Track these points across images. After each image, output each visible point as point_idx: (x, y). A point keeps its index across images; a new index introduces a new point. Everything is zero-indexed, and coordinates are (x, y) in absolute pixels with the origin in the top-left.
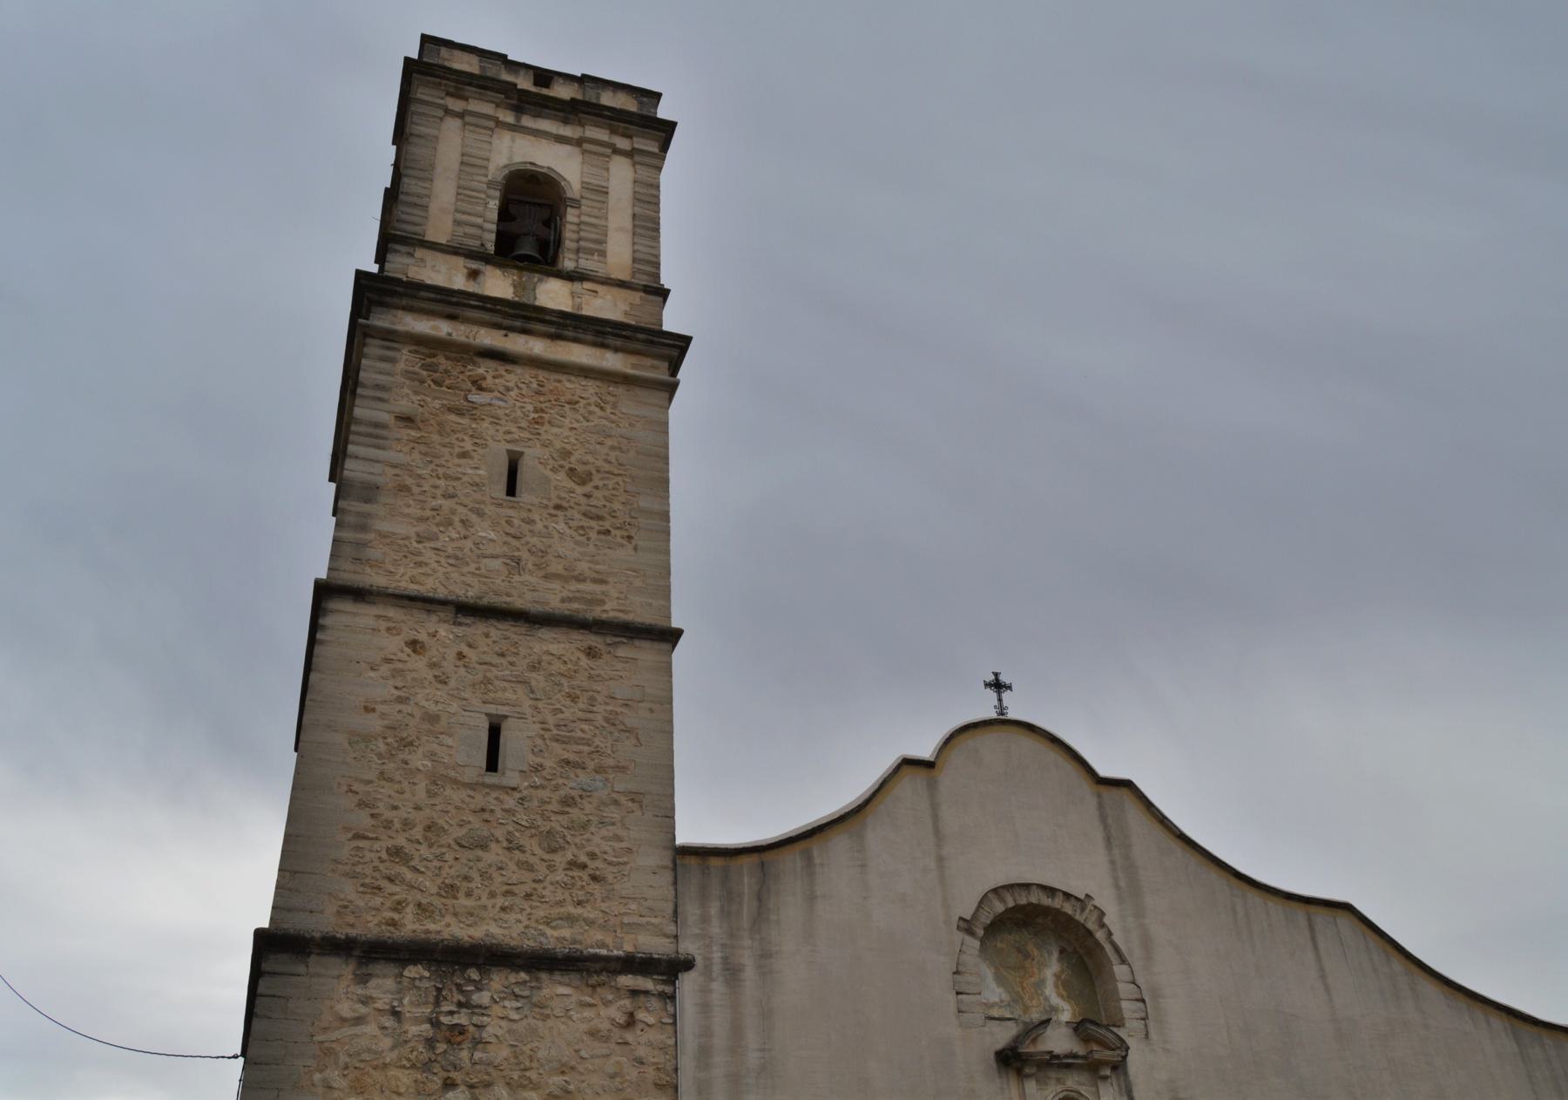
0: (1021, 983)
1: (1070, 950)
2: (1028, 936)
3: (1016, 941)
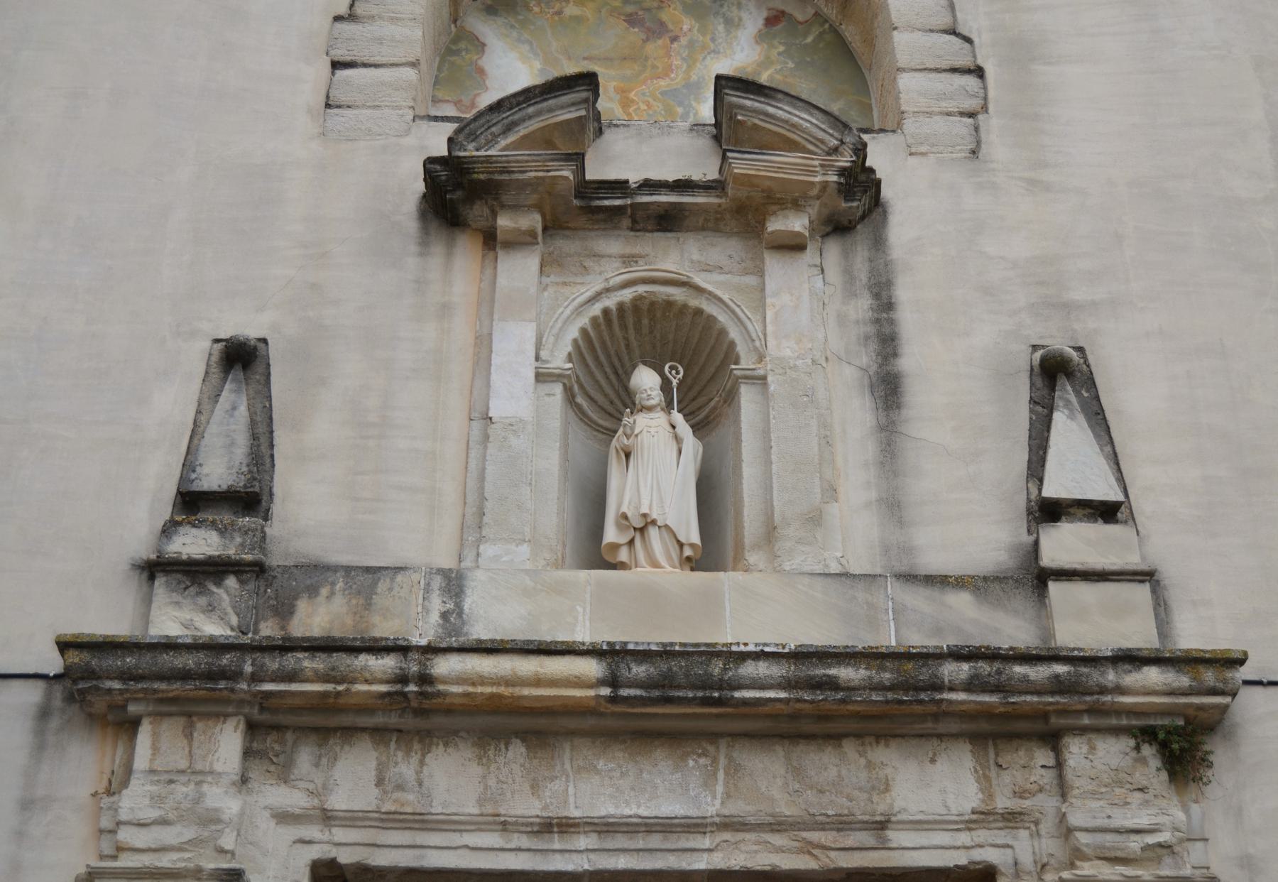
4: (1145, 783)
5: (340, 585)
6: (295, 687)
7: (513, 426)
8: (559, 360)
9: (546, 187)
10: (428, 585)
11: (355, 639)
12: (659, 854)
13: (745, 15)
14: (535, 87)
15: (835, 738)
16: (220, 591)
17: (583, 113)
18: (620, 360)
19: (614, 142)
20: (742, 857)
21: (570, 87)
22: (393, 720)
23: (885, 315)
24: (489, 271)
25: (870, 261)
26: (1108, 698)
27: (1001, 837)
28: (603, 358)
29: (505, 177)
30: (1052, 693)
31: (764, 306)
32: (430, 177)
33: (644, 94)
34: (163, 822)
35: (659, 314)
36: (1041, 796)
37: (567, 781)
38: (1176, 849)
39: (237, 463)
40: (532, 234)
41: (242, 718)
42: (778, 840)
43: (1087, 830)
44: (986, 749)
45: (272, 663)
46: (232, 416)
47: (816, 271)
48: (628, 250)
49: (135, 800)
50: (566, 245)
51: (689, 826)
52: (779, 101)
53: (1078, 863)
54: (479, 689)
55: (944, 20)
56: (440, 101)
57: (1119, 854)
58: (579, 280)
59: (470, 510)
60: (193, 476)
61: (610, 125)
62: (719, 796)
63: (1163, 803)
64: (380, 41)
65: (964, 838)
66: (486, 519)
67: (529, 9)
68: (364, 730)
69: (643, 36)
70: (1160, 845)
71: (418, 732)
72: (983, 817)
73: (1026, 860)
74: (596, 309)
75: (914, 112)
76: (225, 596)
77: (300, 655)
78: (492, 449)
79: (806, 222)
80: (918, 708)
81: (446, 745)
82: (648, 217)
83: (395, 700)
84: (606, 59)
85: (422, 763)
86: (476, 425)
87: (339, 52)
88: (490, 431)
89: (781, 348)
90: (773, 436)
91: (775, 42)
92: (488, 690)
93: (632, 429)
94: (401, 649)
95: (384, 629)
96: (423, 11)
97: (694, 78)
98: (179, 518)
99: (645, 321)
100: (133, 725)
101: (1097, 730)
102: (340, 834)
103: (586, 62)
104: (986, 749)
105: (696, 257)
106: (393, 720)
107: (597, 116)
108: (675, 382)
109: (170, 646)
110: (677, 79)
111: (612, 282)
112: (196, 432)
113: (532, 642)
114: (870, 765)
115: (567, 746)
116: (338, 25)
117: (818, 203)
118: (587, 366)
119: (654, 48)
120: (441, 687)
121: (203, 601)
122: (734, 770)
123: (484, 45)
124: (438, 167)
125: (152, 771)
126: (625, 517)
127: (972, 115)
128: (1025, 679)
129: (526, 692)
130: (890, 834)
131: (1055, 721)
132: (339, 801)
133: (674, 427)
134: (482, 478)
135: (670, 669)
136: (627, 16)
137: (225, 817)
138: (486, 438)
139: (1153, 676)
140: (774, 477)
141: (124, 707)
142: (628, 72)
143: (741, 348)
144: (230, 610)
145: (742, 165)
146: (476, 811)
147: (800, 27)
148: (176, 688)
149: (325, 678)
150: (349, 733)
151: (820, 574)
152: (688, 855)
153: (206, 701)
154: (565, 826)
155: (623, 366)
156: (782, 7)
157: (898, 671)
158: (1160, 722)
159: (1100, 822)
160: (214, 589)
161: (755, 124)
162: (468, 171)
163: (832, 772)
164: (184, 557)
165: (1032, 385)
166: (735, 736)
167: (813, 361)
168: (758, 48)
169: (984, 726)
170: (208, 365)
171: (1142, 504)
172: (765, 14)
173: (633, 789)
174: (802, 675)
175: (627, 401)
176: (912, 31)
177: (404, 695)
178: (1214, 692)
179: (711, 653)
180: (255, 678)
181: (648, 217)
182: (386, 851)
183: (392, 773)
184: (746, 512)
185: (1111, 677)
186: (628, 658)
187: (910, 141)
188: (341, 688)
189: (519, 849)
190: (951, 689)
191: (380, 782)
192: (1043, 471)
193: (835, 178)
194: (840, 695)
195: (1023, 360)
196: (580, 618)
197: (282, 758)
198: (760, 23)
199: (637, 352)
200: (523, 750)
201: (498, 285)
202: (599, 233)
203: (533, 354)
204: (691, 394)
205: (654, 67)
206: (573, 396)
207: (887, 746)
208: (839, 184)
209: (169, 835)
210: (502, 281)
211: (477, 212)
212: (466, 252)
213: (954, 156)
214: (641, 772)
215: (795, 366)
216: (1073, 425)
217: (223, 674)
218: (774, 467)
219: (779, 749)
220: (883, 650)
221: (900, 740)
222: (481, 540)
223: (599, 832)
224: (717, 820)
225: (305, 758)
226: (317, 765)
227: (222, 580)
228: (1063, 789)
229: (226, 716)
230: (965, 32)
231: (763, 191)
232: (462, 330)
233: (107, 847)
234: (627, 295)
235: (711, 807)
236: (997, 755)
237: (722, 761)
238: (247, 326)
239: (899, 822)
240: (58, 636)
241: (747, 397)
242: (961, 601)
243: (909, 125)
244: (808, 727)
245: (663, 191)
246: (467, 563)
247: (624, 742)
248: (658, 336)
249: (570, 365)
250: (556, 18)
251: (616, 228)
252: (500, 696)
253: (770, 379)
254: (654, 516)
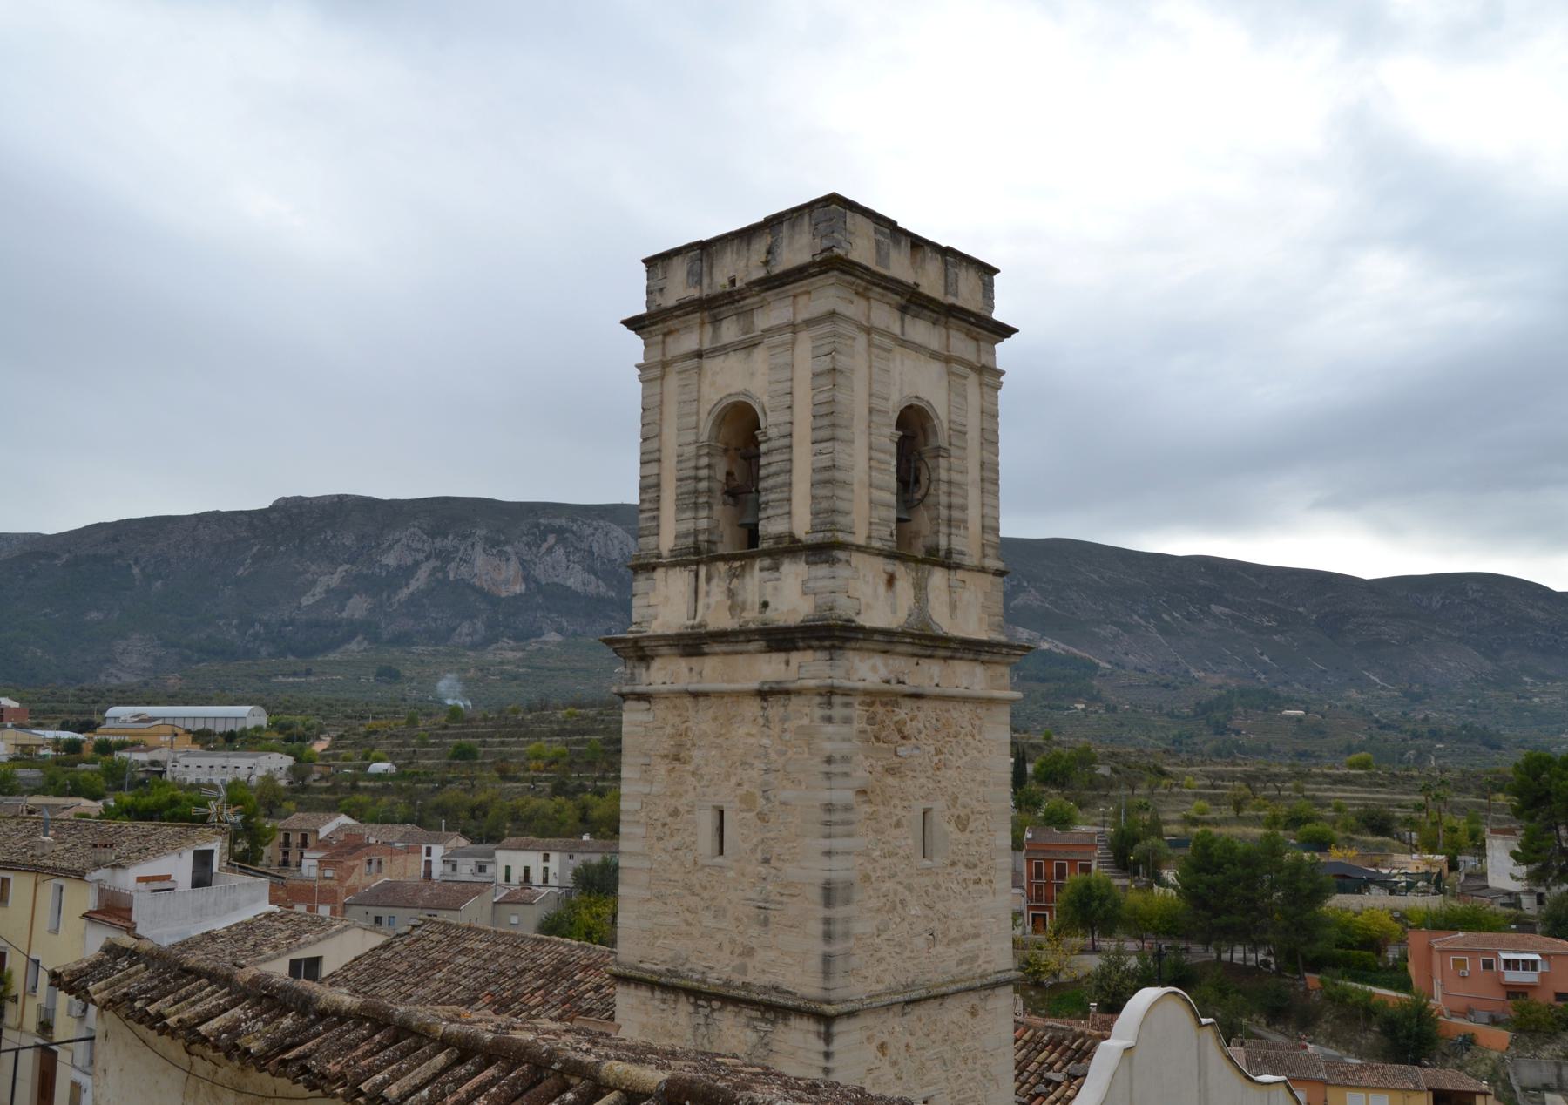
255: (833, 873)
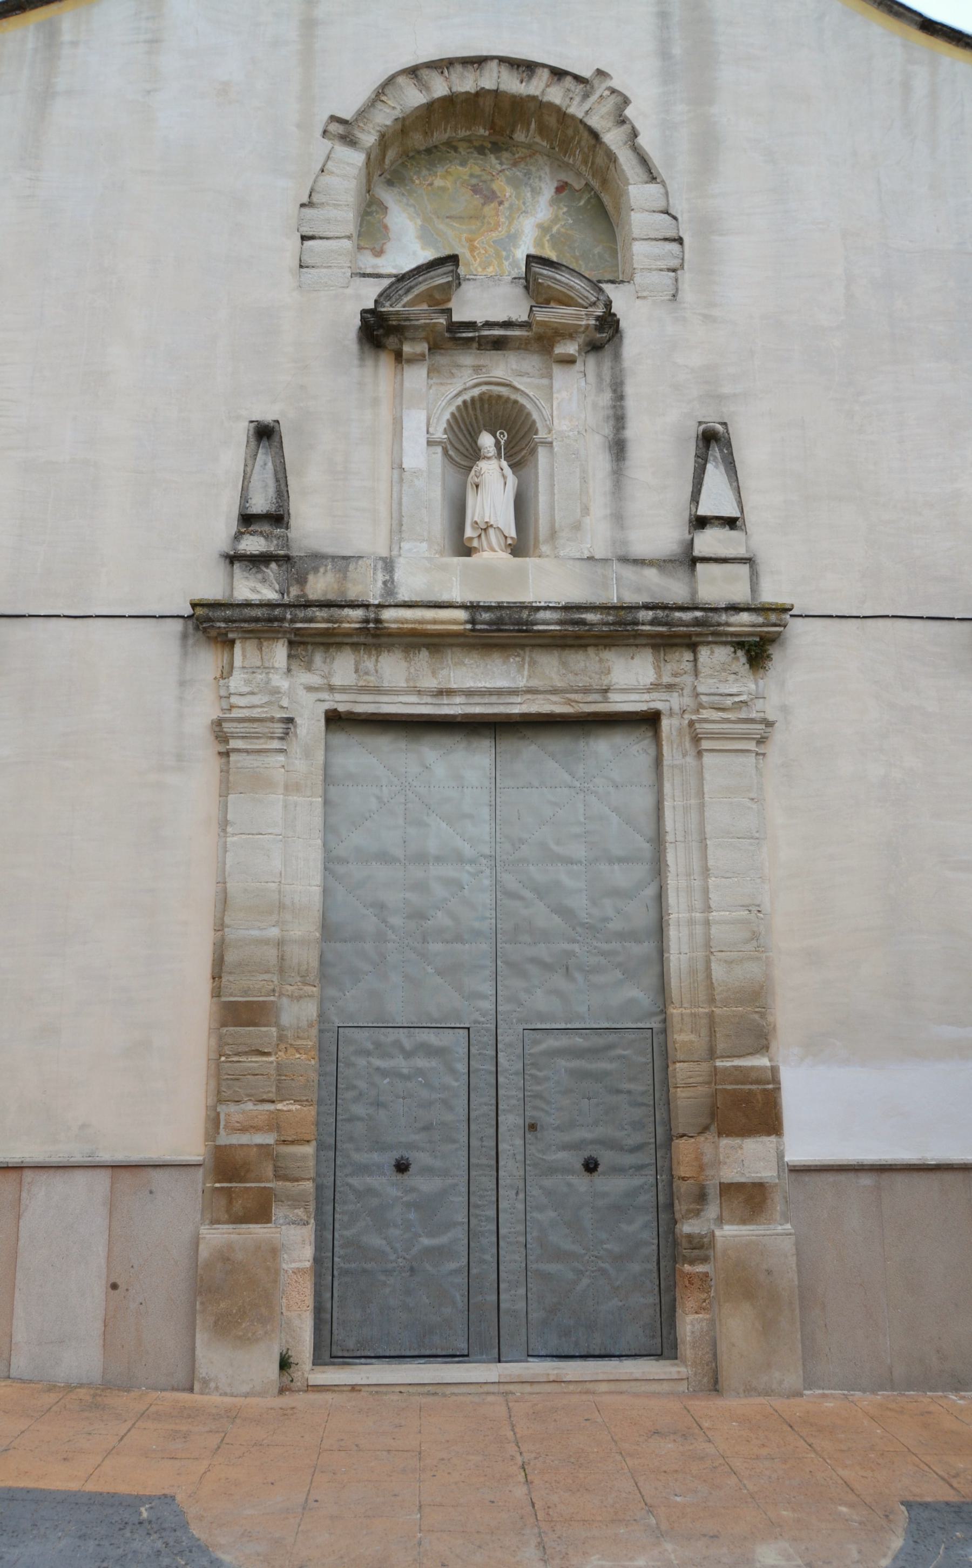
0: (471, 241)
1: (577, 185)
2: (499, 167)
3: (472, 175)
4: (737, 670)
5: (330, 567)
6: (313, 625)
7: (416, 473)
8: (439, 433)
9: (430, 329)
10: (375, 566)
11: (342, 601)
12: (496, 706)
13: (543, 185)
14: (423, 265)
15: (584, 647)
16: (268, 571)
17: (450, 279)
18: (472, 426)
19: (468, 291)
20: (537, 706)
21: (443, 264)
22: (362, 639)
23: (619, 403)
24: (399, 377)
25: (612, 368)
26: (722, 628)
27: (664, 696)
28: (462, 426)
29: (407, 323)
30: (694, 626)
31: (552, 398)
32: (362, 319)
33: (483, 243)
34: (252, 693)
35: (494, 402)
36: (685, 676)
37: (450, 670)
38: (749, 703)
39: (270, 497)
40: (423, 355)
41: (286, 640)
42: (554, 698)
43: (706, 694)
44: (659, 652)
45: (301, 614)
46: (264, 469)
47: (582, 375)
48: (477, 363)
49: (237, 682)
50: (442, 360)
51: (510, 692)
52: (563, 271)
53: (701, 710)
54: (405, 626)
55: (661, 204)
56: (362, 248)
57: (721, 706)
58: (449, 381)
59: (395, 522)
60: (248, 505)
61: (466, 279)
62: (525, 677)
63: (745, 680)
64: (328, 221)
65: (646, 697)
66: (404, 528)
67: (413, 182)
68: (347, 644)
69: (482, 201)
70: (741, 702)
71: (374, 645)
72: (656, 687)
73: (676, 708)
74: (459, 401)
75: (641, 269)
76: (271, 573)
77: (314, 609)
78: (405, 487)
79: (577, 347)
80: (626, 633)
81: (389, 651)
82: (488, 342)
83: (363, 631)
84: (461, 218)
85: (377, 661)
86: (396, 472)
87: (305, 229)
88: (404, 477)
89: (562, 425)
90: (555, 479)
91: (561, 205)
92: (410, 626)
93: (480, 473)
94: (366, 606)
95: (353, 593)
96: (352, 199)
97: (513, 231)
98: (243, 530)
99: (486, 406)
100: (232, 642)
101: (716, 643)
102: (338, 697)
103: (448, 220)
104: (659, 652)
105: (514, 367)
106: (362, 639)
107: (458, 277)
108: (502, 442)
109: (248, 605)
110: (501, 233)
111: (468, 385)
112: (246, 478)
113: (431, 602)
114: (601, 661)
115: (449, 651)
116: (303, 210)
117: (583, 335)
118: (454, 432)
119: (488, 210)
120: (386, 625)
121: (260, 576)
122: (533, 663)
123: (386, 208)
124: (369, 316)
125: (244, 668)
126: (476, 523)
127: (674, 270)
128: (680, 619)
129: (429, 627)
130: (610, 695)
131: (694, 639)
132: (337, 681)
133: (502, 470)
134: (400, 504)
135: (501, 615)
136: (472, 186)
137: (282, 691)
138: (401, 480)
139: (745, 617)
140: (556, 503)
141: (226, 634)
142: (474, 227)
143: (539, 425)
144: (274, 581)
145: (542, 315)
146: (405, 685)
147: (577, 194)
148: (253, 626)
149: (328, 621)
150: (340, 645)
151: (579, 559)
152: (510, 706)
153: (267, 631)
154: (450, 692)
155: (473, 429)
156: (566, 180)
157: (617, 616)
158: (747, 639)
159: (712, 691)
160: (265, 569)
161: (549, 285)
162: (387, 320)
163: (582, 664)
164: (248, 553)
165: (697, 446)
166: (534, 646)
167: (578, 432)
168: (551, 209)
169: (659, 641)
170: (248, 437)
171: (751, 518)
172: (555, 185)
173: (482, 673)
174: (568, 618)
175: (475, 454)
176: (643, 212)
177: (368, 629)
178: (775, 625)
179: (522, 607)
180: (292, 621)
181: (488, 342)
182: (362, 705)
183: (361, 667)
184: (541, 521)
185: (724, 617)
186: (480, 609)
187: (638, 288)
188: (336, 626)
189: (427, 704)
190: (643, 624)
191: (357, 671)
192: (699, 497)
193: (593, 322)
194: (587, 628)
195: (693, 431)
196: (455, 584)
197: (306, 658)
198: (553, 190)
199: (481, 422)
200: (427, 654)
201: (404, 386)
202: (460, 351)
203: (425, 429)
204: (511, 445)
205: (489, 223)
206: (447, 451)
207: (610, 650)
208: (596, 325)
209: (255, 700)
210: (407, 384)
211: (392, 341)
212: (386, 361)
213: (662, 298)
214: (487, 665)
215: (569, 436)
216: (717, 472)
217: (276, 619)
218: (556, 497)
219: (555, 652)
220: (609, 605)
221: (616, 648)
222: (401, 540)
223: (466, 695)
224: (524, 689)
225: (318, 658)
226: (325, 662)
227: (269, 564)
228: (696, 673)
229: (278, 638)
230: (674, 214)
231: (553, 329)
232: (385, 413)
233: (225, 705)
234: (476, 392)
235: (522, 683)
236: (665, 655)
237: (527, 659)
238: (268, 417)
239: (614, 689)
240: (191, 600)
241: (542, 453)
242: (651, 574)
243: (638, 278)
244: (569, 642)
245: (497, 327)
246: (395, 553)
247: (478, 649)
248: (493, 413)
249: (446, 436)
250: (430, 188)
251: (469, 348)
252: (416, 629)
253: (554, 444)
254: (492, 523)
255: (600, 463)
